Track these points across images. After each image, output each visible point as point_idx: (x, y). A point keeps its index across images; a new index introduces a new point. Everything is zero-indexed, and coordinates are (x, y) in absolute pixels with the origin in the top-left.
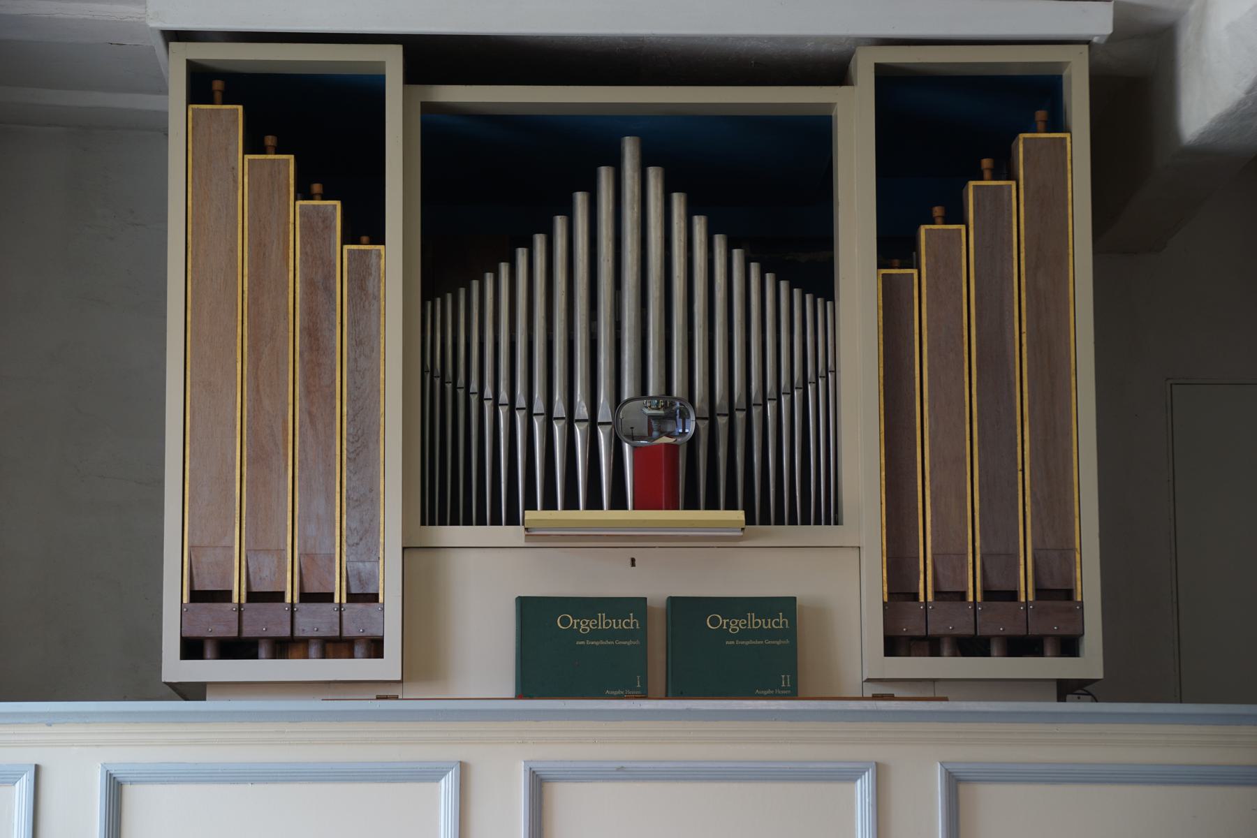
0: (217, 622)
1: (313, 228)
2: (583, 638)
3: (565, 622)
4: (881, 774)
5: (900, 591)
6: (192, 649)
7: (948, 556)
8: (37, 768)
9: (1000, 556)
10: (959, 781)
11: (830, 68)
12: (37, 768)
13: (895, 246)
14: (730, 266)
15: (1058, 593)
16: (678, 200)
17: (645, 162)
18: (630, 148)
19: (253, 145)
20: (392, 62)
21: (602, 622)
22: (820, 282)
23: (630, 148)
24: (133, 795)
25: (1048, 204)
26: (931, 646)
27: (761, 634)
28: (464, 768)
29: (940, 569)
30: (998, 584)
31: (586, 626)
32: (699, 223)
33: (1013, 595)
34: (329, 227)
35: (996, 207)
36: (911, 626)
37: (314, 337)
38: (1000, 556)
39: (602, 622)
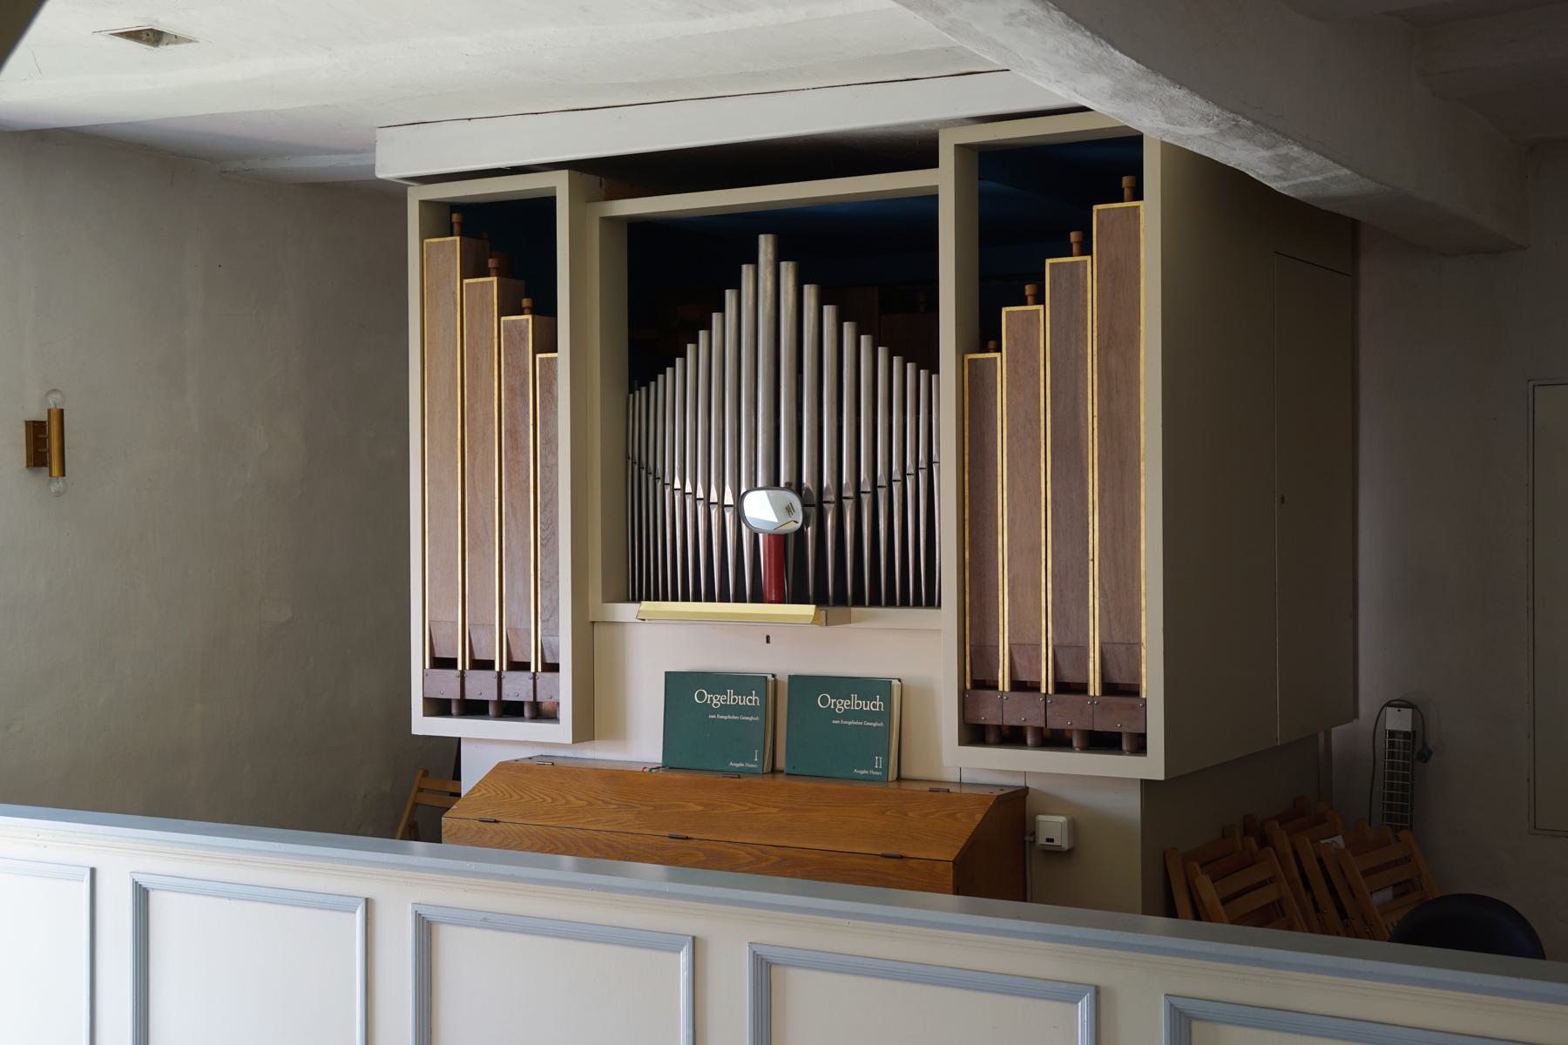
0: (447, 685)
1: (515, 341)
2: (715, 712)
3: (701, 696)
4: (696, 946)
5: (976, 679)
6: (437, 707)
7: (1024, 648)
8: (93, 871)
9: (1070, 649)
10: (770, 965)
11: (914, 150)
12: (93, 871)
13: (984, 333)
14: (858, 348)
15: (1121, 689)
16: (810, 292)
17: (780, 255)
18: (766, 245)
19: (474, 267)
20: (560, 183)
21: (731, 698)
22: (930, 363)
23: (766, 245)
24: (154, 898)
25: (1121, 281)
26: (1012, 737)
27: (861, 715)
28: (368, 903)
29: (1016, 658)
30: (1069, 676)
31: (717, 701)
32: (829, 311)
33: (1082, 689)
34: (524, 340)
35: (1074, 279)
36: (989, 714)
37: (515, 435)
38: (1070, 649)
39: (731, 698)
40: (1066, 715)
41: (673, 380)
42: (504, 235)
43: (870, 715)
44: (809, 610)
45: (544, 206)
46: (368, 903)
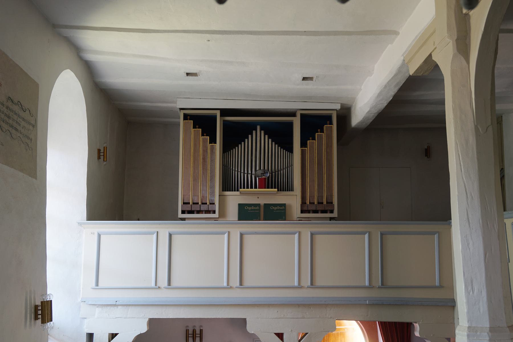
0: (188, 208)
1: (204, 141)
4: (300, 233)
5: (303, 202)
6: (183, 212)
9: (320, 197)
11: (293, 114)
13: (303, 144)
18: (258, 127)
20: (218, 113)
22: (290, 149)
23: (258, 127)
26: (308, 212)
28: (229, 232)
30: (320, 201)
31: (250, 208)
32: (270, 140)
33: (322, 203)
34: (207, 141)
35: (320, 138)
36: (305, 208)
37: (204, 159)
38: (320, 197)
39: (253, 208)
40: (320, 208)
41: (235, 151)
42: (202, 122)
43: (281, 210)
44: (276, 190)
45: (214, 118)
46: (229, 232)
